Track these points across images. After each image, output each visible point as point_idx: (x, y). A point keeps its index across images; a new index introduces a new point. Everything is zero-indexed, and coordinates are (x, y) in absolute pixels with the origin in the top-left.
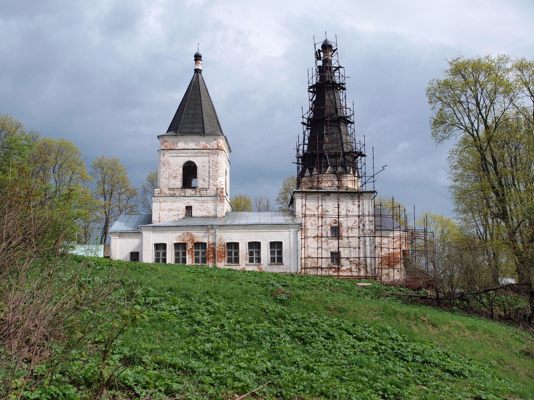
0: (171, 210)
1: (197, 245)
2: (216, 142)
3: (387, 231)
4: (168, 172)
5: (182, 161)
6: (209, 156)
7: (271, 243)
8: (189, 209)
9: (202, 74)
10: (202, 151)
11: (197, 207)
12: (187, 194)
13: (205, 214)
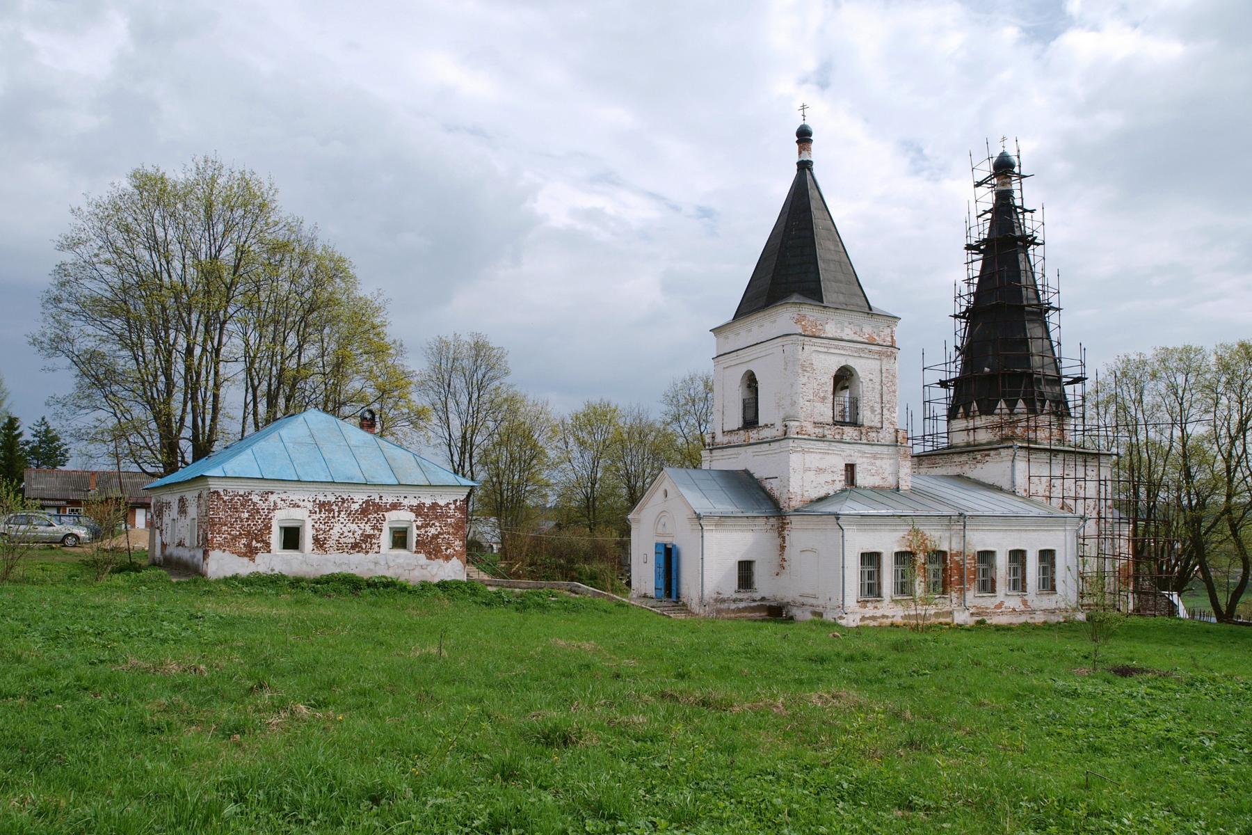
0: (820, 470)
7: (1041, 552)
8: (850, 469)
9: (815, 171)
13: (876, 481)
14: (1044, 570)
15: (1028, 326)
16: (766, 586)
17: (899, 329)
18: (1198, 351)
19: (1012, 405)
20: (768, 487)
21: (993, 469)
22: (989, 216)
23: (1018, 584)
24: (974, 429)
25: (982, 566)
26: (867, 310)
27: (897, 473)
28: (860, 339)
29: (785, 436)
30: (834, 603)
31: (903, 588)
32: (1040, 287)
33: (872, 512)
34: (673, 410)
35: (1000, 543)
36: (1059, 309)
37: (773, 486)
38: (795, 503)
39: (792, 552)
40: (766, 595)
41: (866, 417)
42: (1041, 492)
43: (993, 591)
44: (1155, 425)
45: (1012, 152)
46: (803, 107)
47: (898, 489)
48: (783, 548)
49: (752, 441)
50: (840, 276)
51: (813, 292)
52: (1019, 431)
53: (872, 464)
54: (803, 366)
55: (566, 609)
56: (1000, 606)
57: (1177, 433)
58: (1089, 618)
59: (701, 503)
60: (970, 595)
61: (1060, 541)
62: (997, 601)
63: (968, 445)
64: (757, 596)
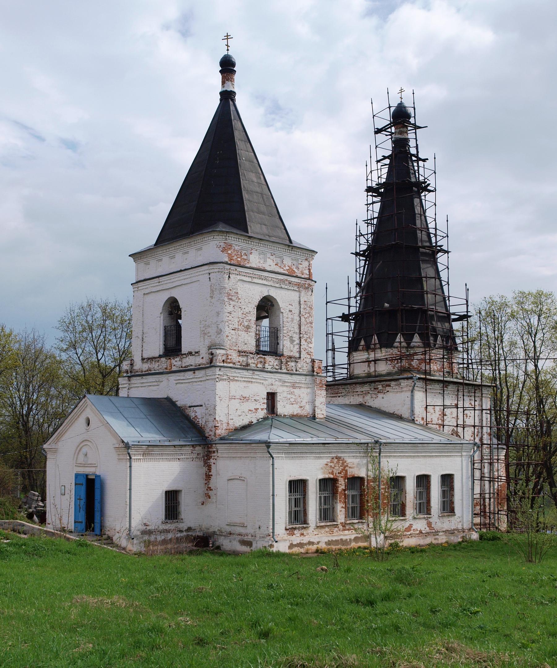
0: (244, 399)
1: (355, 482)
6: (299, 291)
8: (271, 397)
9: (237, 103)
13: (295, 410)
14: (444, 493)
15: (423, 266)
16: (191, 516)
17: (316, 261)
18: (549, 296)
19: (409, 338)
20: (192, 415)
21: (393, 399)
22: (387, 161)
23: (424, 507)
24: (375, 361)
25: (394, 492)
26: (287, 242)
27: (313, 402)
28: (281, 271)
29: (211, 364)
30: (264, 531)
31: (327, 515)
32: (432, 231)
33: (299, 440)
34: (69, 336)
35: (408, 468)
36: (447, 252)
37: (198, 414)
38: (221, 432)
39: (218, 482)
40: (192, 525)
41: (287, 347)
42: (435, 421)
43: (403, 514)
44: (513, 360)
45: (408, 103)
46: (227, 37)
47: (314, 417)
48: (208, 477)
49: (174, 369)
50: (263, 208)
51: (237, 222)
52: (415, 363)
53: (292, 393)
54: (229, 295)
55: (25, 552)
56: (409, 528)
57: (531, 367)
58: (481, 537)
59: (129, 432)
60: (384, 519)
61: (457, 465)
62: (407, 525)
63: (369, 375)
64: (184, 526)
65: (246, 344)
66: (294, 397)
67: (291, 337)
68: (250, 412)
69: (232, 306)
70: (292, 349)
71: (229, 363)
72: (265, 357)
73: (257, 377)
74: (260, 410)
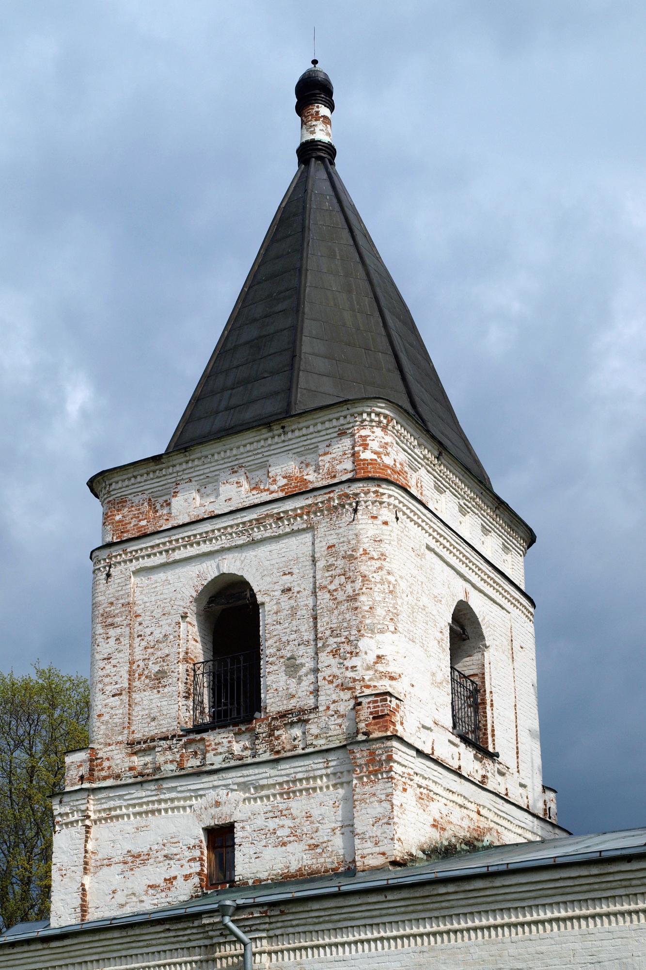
2: (347, 442)
3: (333, 414)
4: (124, 657)
5: (187, 583)
8: (221, 838)
10: (275, 509)
11: (260, 822)
12: (215, 760)
65: (154, 719)
66: (288, 822)
67: (292, 658)
68: (151, 891)
69: (112, 641)
70: (292, 691)
71: (105, 778)
72: (204, 735)
73: (173, 795)
74: (180, 879)
